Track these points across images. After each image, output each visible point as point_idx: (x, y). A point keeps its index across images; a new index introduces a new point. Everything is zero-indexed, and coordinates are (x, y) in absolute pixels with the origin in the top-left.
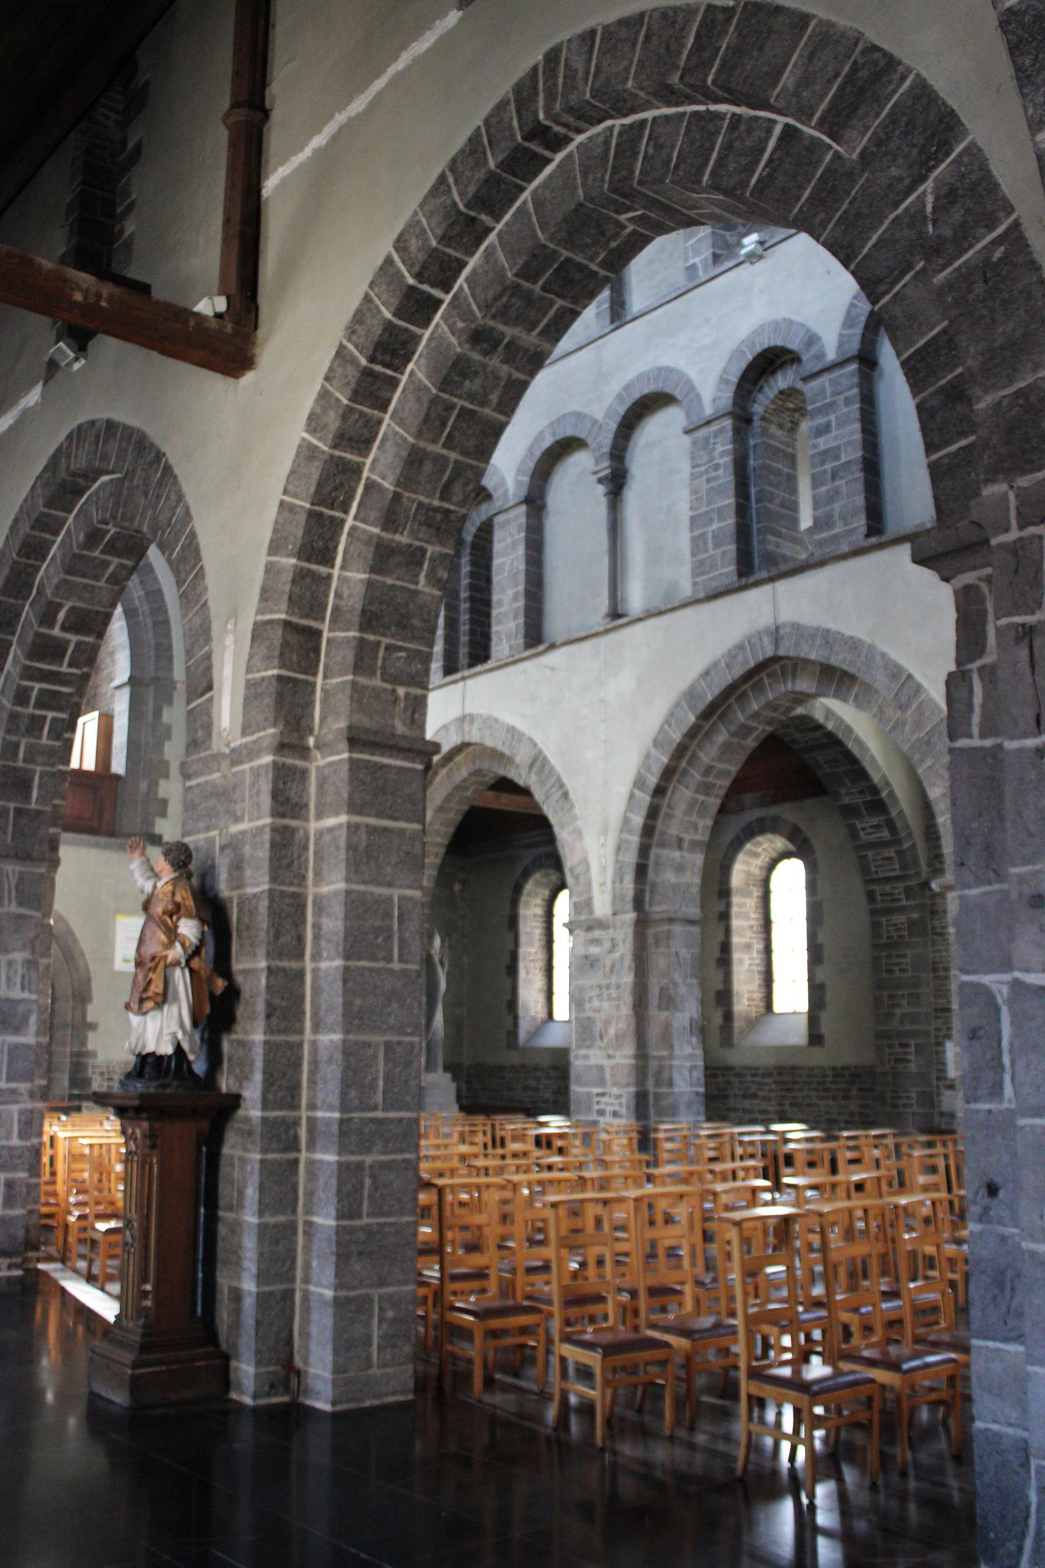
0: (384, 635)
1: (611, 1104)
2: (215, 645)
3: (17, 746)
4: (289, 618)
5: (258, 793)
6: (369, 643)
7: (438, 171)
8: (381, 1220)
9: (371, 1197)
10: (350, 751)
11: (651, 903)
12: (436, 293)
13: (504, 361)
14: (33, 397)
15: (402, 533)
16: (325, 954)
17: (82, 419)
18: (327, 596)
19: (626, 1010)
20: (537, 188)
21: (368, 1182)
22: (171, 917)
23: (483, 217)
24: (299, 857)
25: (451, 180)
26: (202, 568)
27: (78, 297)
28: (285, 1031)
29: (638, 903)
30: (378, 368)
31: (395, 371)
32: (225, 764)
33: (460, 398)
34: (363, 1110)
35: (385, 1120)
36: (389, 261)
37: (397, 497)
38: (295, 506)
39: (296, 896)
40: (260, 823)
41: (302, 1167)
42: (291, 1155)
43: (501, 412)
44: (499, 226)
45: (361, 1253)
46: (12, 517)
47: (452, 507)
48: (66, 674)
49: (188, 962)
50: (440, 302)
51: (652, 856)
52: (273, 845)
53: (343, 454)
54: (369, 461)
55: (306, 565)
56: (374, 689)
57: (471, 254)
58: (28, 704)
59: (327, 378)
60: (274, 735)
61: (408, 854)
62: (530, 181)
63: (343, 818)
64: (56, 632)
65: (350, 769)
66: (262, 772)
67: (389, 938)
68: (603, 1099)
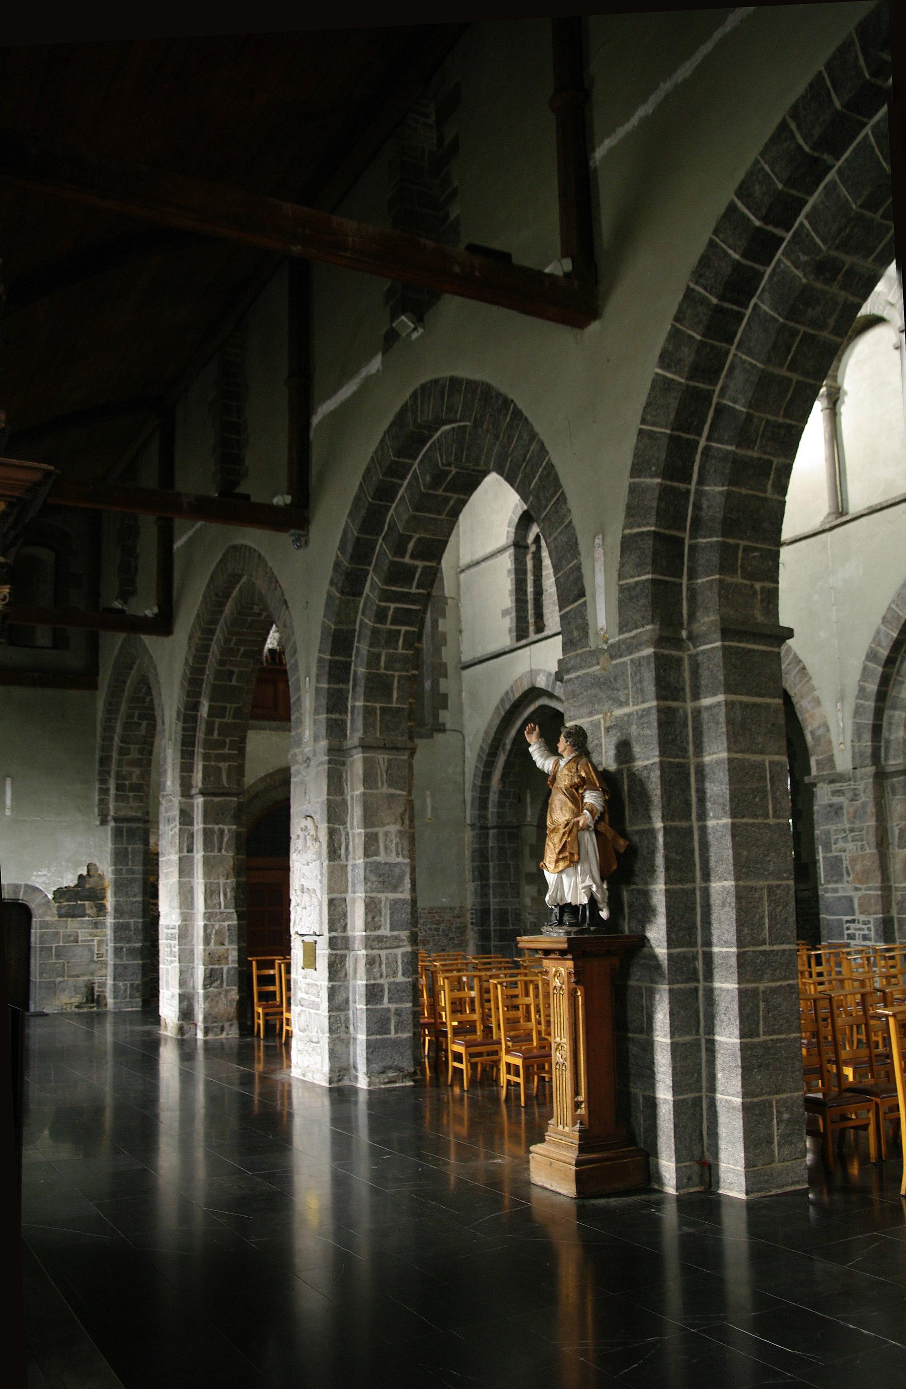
0: (742, 539)
1: (860, 929)
2: (583, 559)
3: (379, 656)
4: (658, 530)
5: (641, 681)
6: (730, 545)
7: (778, 120)
8: (774, 1037)
9: (765, 1017)
10: (722, 641)
11: (886, 759)
12: (778, 232)
13: (843, 287)
14: (375, 365)
15: (753, 449)
16: (711, 814)
17: (423, 380)
18: (687, 509)
19: (871, 850)
20: (878, 122)
21: (762, 1005)
22: (577, 790)
23: (826, 156)
24: (681, 732)
25: (793, 126)
26: (563, 493)
27: (457, 269)
28: (680, 881)
29: (876, 757)
30: (727, 305)
31: (741, 306)
32: (604, 658)
33: (804, 324)
34: (754, 945)
35: (772, 951)
36: (732, 208)
37: (749, 417)
38: (655, 432)
39: (679, 765)
40: (646, 705)
41: (701, 993)
42: (692, 985)
43: (837, 334)
44: (839, 164)
45: (760, 1066)
46: (364, 467)
47: (793, 423)
48: (415, 594)
49: (595, 825)
50: (783, 239)
51: (885, 718)
52: (661, 724)
53: (696, 384)
54: (717, 389)
55: (669, 483)
56: (737, 585)
57: (811, 192)
58: (386, 621)
59: (677, 319)
60: (653, 630)
61: (773, 725)
62: (870, 117)
63: (721, 698)
64: (407, 560)
65: (724, 656)
66: (644, 663)
67: (765, 797)
68: (852, 925)
